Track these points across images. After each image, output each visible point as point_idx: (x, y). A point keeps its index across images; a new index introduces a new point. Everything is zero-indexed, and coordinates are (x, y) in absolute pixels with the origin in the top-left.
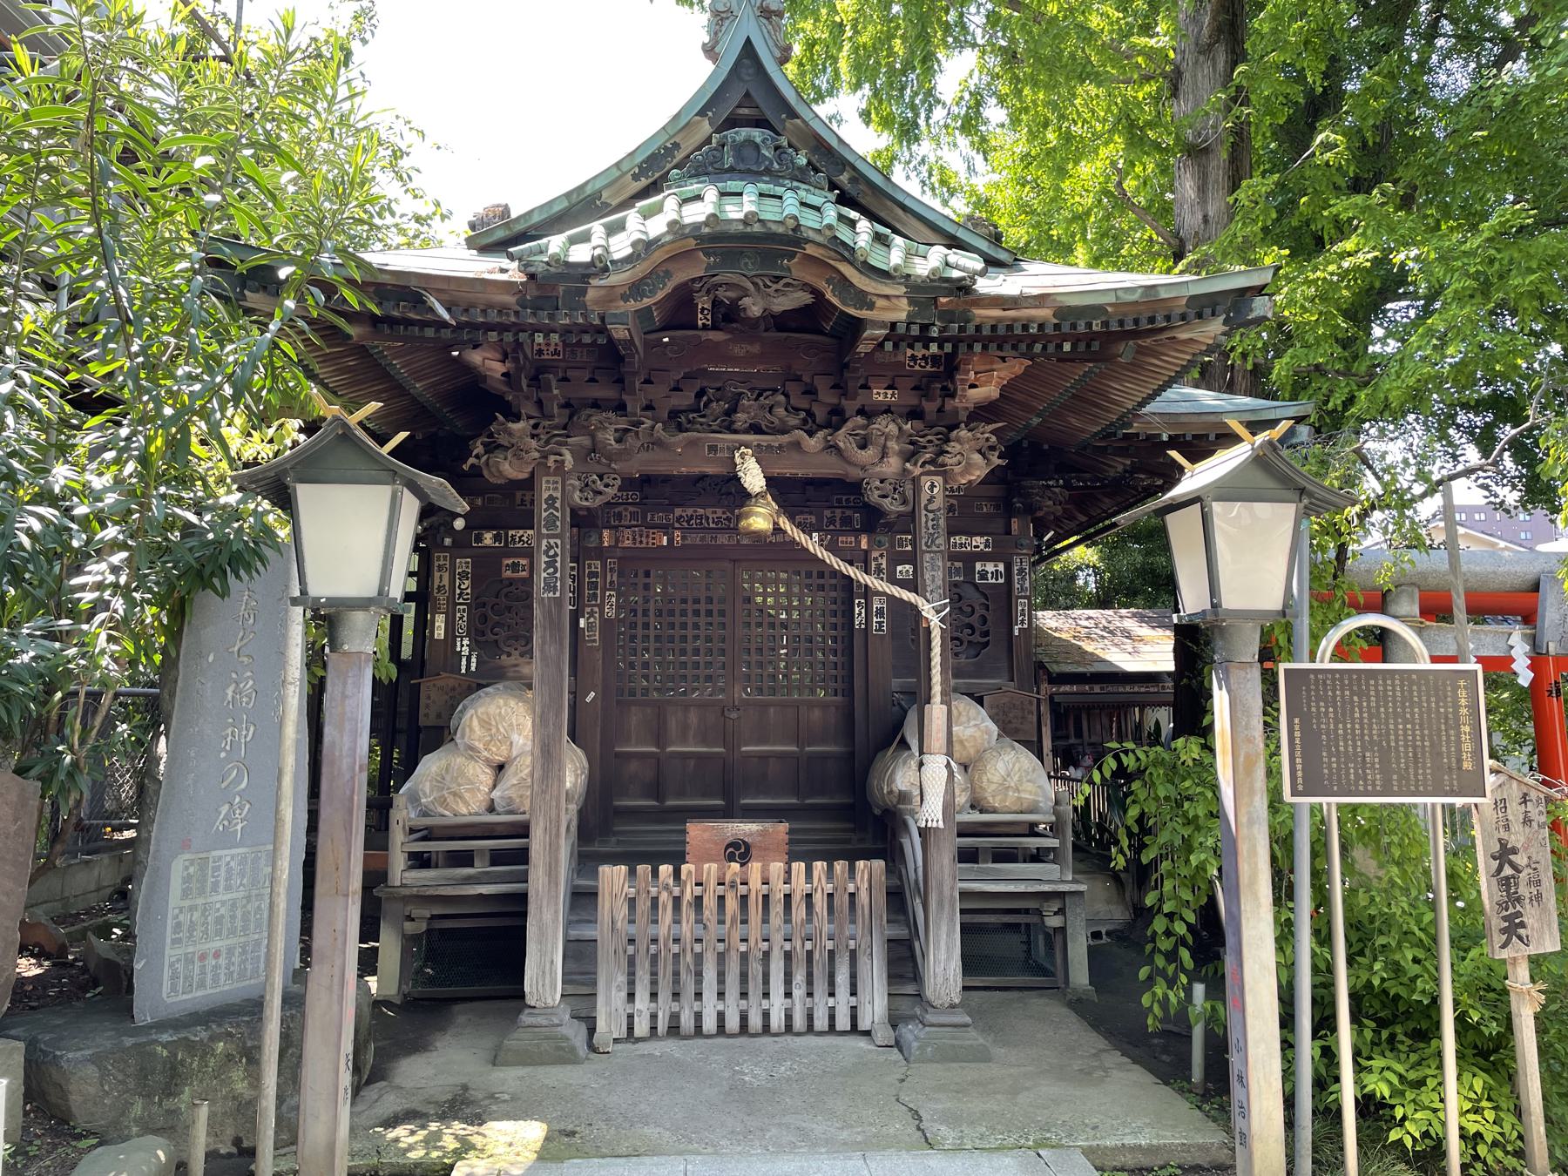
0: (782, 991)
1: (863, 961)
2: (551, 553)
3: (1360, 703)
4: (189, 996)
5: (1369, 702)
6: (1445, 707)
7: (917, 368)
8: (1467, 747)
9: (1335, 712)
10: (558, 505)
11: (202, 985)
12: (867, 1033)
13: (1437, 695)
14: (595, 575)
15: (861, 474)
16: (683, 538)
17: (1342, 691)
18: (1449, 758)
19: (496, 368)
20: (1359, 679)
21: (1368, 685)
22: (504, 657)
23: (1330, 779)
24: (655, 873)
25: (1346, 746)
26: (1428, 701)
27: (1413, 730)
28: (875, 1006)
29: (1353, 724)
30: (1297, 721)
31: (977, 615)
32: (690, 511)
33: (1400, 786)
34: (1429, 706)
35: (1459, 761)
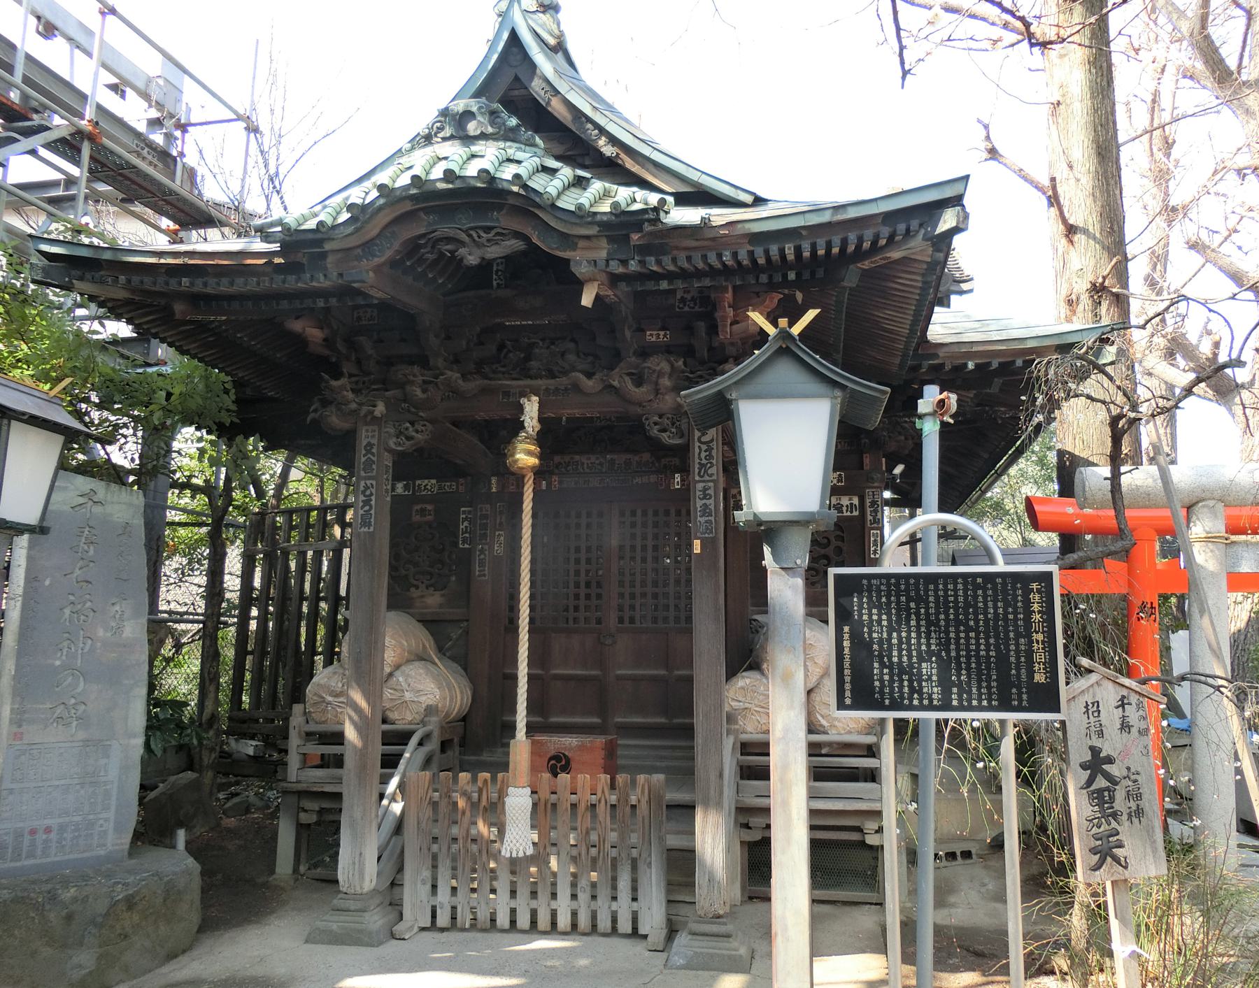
0: (568, 892)
1: (642, 866)
2: (368, 493)
3: (918, 609)
4: (18, 864)
5: (927, 608)
6: (1015, 613)
7: (686, 309)
8: (1040, 656)
9: (889, 620)
10: (374, 450)
11: (31, 855)
12: (645, 937)
13: (1005, 600)
14: (486, 517)
15: (639, 410)
16: (560, 482)
17: (898, 596)
18: (1018, 669)
19: (315, 334)
20: (917, 584)
21: (927, 590)
22: (413, 589)
23: (882, 692)
24: (455, 779)
25: (900, 656)
26: (996, 608)
27: (977, 638)
28: (653, 918)
29: (909, 632)
30: (846, 629)
31: (832, 547)
32: (567, 458)
33: (960, 699)
34: (995, 612)
35: (1031, 673)
